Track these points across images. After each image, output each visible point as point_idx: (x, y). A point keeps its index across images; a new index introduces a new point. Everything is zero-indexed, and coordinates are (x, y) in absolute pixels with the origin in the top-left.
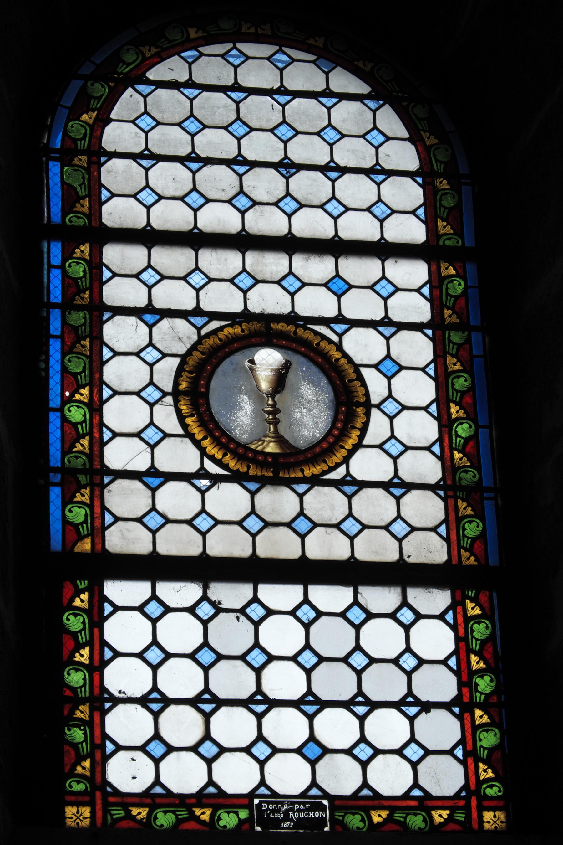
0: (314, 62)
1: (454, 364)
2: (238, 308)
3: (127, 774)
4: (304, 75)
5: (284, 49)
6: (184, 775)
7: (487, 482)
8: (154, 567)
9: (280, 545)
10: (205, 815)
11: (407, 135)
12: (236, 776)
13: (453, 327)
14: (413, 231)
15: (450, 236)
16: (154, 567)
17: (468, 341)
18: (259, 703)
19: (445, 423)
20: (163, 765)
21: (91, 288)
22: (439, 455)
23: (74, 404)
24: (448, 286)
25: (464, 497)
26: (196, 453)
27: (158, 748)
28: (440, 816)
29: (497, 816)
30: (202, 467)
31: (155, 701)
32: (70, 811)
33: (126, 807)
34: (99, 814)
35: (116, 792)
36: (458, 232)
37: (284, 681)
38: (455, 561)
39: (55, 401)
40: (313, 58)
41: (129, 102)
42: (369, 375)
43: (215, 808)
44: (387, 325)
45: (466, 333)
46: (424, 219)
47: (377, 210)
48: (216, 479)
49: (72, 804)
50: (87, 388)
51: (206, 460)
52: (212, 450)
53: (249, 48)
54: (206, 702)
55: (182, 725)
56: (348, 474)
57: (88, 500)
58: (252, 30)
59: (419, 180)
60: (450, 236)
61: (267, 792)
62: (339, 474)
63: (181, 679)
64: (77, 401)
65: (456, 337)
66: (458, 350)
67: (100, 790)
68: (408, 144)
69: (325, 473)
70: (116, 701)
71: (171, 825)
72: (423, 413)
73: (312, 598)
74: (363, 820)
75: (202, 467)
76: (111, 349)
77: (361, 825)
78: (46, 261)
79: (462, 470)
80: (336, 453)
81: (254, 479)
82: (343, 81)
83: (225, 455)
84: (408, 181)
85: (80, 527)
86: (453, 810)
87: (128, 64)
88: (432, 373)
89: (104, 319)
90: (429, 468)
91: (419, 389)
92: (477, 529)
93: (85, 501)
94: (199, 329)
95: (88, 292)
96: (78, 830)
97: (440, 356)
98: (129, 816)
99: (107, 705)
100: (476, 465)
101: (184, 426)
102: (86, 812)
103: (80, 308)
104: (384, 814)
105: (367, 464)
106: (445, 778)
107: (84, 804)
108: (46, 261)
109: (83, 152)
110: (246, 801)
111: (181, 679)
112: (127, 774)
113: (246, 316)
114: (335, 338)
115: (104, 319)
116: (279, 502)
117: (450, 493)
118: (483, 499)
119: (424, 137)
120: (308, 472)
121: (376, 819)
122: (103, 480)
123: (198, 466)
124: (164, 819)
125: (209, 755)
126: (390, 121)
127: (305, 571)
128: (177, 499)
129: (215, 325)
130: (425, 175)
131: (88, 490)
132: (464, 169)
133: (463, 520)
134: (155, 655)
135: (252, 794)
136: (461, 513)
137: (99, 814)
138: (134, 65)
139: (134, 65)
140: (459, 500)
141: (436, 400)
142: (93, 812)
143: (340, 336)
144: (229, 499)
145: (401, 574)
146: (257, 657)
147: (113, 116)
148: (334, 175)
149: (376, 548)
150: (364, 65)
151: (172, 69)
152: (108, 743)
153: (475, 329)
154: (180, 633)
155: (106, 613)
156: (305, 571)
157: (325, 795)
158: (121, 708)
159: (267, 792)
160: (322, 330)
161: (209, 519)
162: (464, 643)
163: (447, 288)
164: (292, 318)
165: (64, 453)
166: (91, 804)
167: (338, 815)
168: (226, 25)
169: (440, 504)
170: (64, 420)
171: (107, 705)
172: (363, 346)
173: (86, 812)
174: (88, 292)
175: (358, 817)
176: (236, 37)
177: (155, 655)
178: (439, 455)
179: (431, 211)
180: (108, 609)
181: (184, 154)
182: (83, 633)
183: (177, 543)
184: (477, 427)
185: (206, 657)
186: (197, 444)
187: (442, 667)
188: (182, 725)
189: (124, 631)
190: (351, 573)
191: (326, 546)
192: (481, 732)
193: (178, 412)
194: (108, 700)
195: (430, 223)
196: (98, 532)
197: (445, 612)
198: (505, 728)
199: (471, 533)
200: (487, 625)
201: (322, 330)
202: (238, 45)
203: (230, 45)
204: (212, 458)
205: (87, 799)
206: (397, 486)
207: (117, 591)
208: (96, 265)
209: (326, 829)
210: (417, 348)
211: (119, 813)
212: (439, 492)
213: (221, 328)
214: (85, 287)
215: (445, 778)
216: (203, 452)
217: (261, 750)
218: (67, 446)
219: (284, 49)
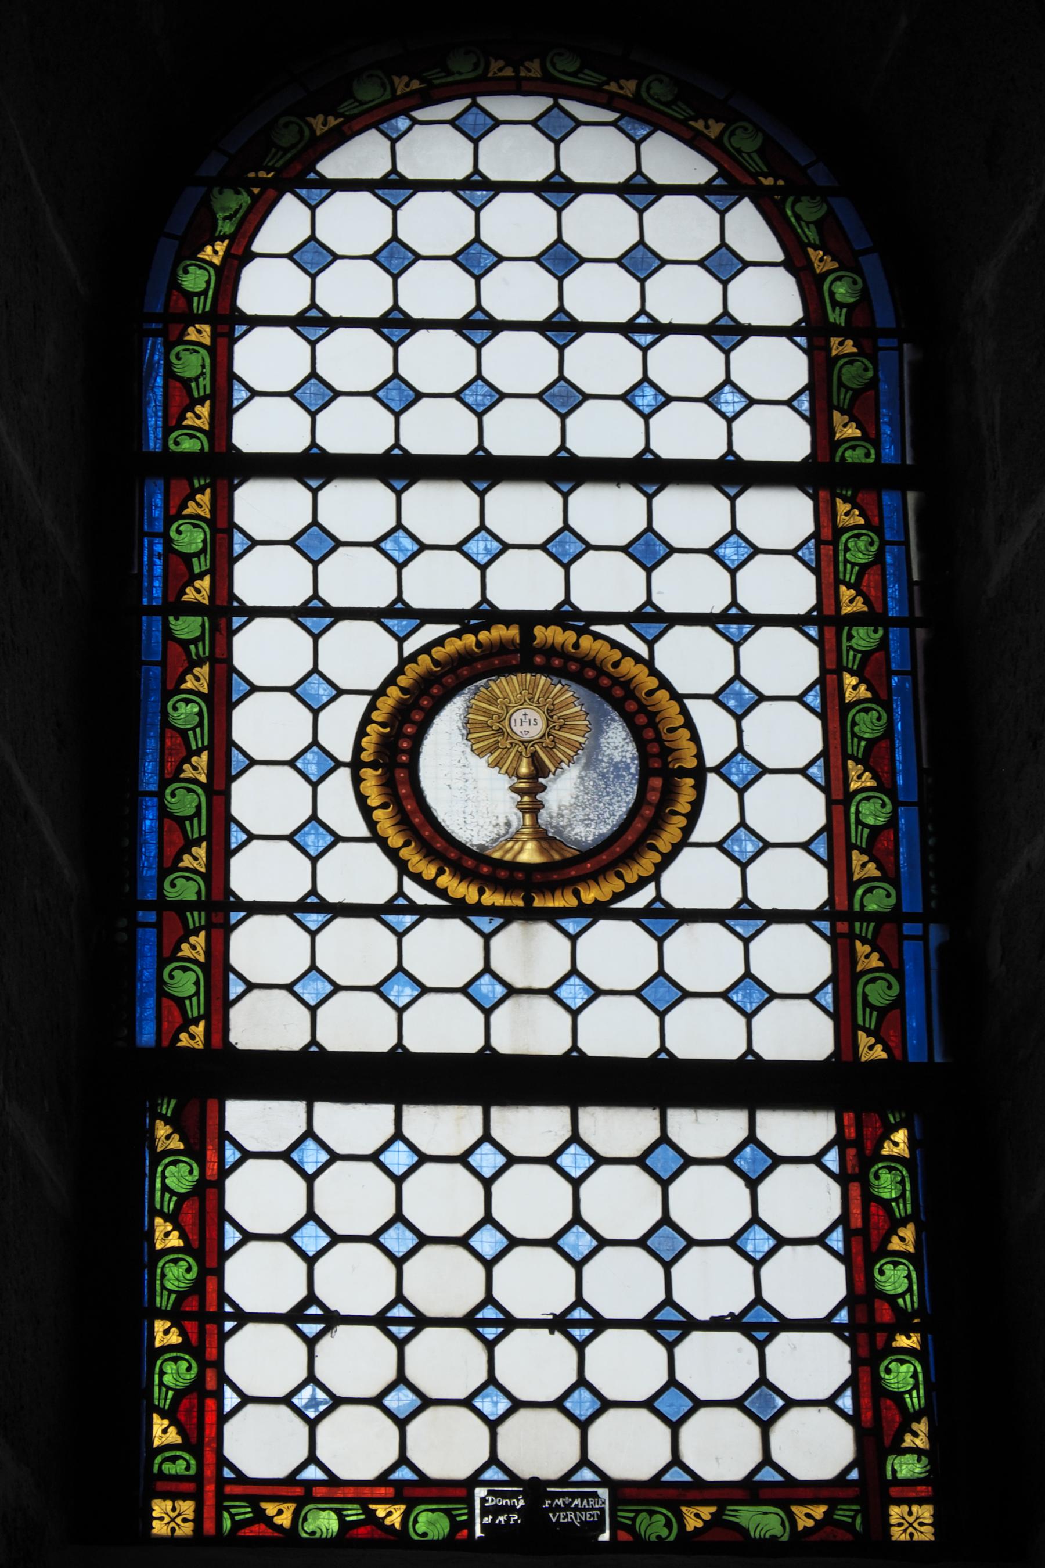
0: (613, 124)
1: (853, 688)
2: (466, 599)
3: (259, 1446)
4: (598, 151)
5: (562, 102)
6: (358, 1448)
7: (913, 904)
8: (314, 1075)
9: (533, 1031)
10: (393, 1515)
11: (780, 257)
12: (448, 1448)
13: (856, 620)
14: (787, 439)
15: (853, 443)
16: (314, 1075)
17: (884, 644)
18: (489, 1322)
19: (838, 799)
20: (323, 1429)
21: (207, 1017)
22: (826, 859)
23: (183, 785)
24: (867, 990)
25: (864, 846)
26: (390, 871)
27: (315, 1404)
28: (808, 1515)
29: (915, 1514)
30: (400, 893)
31: (310, 1318)
32: (160, 1508)
33: (254, 1501)
34: (209, 1512)
35: (241, 1478)
36: (871, 438)
37: (534, 1284)
38: (847, 1057)
39: (149, 780)
40: (612, 116)
41: (286, 223)
42: (703, 713)
43: (411, 1504)
44: (735, 622)
45: (881, 632)
46: (807, 414)
47: (727, 552)
48: (424, 912)
49: (164, 1496)
50: (207, 579)
51: (406, 880)
52: (415, 861)
53: (498, 106)
54: (401, 1322)
55: (356, 1360)
56: (658, 898)
57: (203, 955)
58: (509, 72)
59: (802, 340)
60: (853, 443)
61: (501, 1476)
62: (640, 900)
63: (355, 1281)
64: (187, 869)
65: (864, 638)
66: (853, 400)
67: (215, 1480)
68: (781, 270)
69: (618, 897)
70: (243, 1318)
71: (330, 1535)
72: (817, 1249)
73: (586, 1132)
74: (668, 1524)
75: (400, 893)
76: (244, 829)
77: (664, 1533)
78: (137, 527)
79: (858, 708)
80: (631, 676)
81: (492, 911)
82: (670, 160)
83: (440, 872)
84: (802, 930)
85: (187, 823)
86: (833, 1505)
87: (286, 151)
88: (822, 852)
89: (237, 334)
90: (806, 884)
91: (790, 735)
92: (888, 992)
93: (202, 514)
94: (401, 641)
95: (202, 1024)
96: (172, 1541)
97: (831, 672)
98: (261, 1517)
99: (228, 1326)
100: (890, 876)
101: (371, 824)
102: (187, 1507)
103: (194, 609)
104: (706, 1512)
105: (696, 878)
106: (818, 1447)
107: (185, 1497)
108: (137, 527)
109: (203, 319)
110: (461, 1492)
111: (355, 1281)
112: (259, 1446)
113: (486, 614)
114: (642, 650)
115: (237, 334)
116: (532, 951)
117: (842, 927)
118: (902, 938)
119: (813, 258)
120: (589, 896)
121: (692, 1524)
122: (233, 330)
123: (393, 890)
124: (324, 1522)
125: (399, 1229)
126: (749, 229)
127: (575, 1080)
128: (356, 950)
129: (431, 632)
130: (811, 332)
131: (206, 668)
132: (885, 316)
133: (837, 362)
134: (310, 1237)
135: (474, 1480)
136: (842, 520)
137: (209, 1512)
138: (294, 151)
139: (294, 151)
140: (860, 1033)
141: (833, 979)
142: (199, 1511)
143: (651, 644)
144: (444, 949)
145: (750, 1083)
146: (487, 1241)
147: (256, 247)
148: (645, 339)
149: (706, 1034)
150: (707, 127)
151: (362, 156)
152: (228, 1391)
153: (897, 622)
154: (355, 1198)
155: (228, 1244)
156: (575, 1080)
157: (605, 1480)
158: (251, 1329)
159: (501, 1476)
160: (619, 633)
161: (409, 1234)
162: (868, 1369)
163: (858, 812)
164: (566, 615)
165: (167, 431)
166: (197, 1497)
167: (625, 1515)
168: (463, 67)
169: (824, 950)
170: (164, 813)
171: (228, 1326)
172: (691, 661)
173: (187, 1507)
174: (202, 1024)
175: (660, 1520)
176: (475, 88)
177: (310, 1237)
178: (826, 859)
179: (820, 400)
180: (231, 1237)
181: (377, 175)
182: (196, 821)
183: (357, 1028)
184: (896, 804)
185: (401, 1400)
186: (392, 854)
187: (827, 1412)
188: (356, 1360)
189: (258, 1196)
190: (662, 1082)
191: (619, 1032)
192: (850, 538)
193: (361, 800)
194: (229, 1317)
195: (819, 423)
196: (218, 1007)
197: (839, 1392)
198: (929, 1311)
199: (862, 643)
200: (903, 1177)
201: (619, 633)
202: (482, 101)
203: (467, 102)
204: (417, 878)
205: (191, 1487)
206: (746, 917)
207: (251, 1120)
208: (222, 526)
209: (605, 1537)
210: (787, 661)
211: (244, 1512)
212: (798, 339)
213: (440, 641)
214: (197, 925)
215: (818, 1447)
216: (403, 869)
217: (488, 1242)
218: (169, 768)
219: (562, 102)
